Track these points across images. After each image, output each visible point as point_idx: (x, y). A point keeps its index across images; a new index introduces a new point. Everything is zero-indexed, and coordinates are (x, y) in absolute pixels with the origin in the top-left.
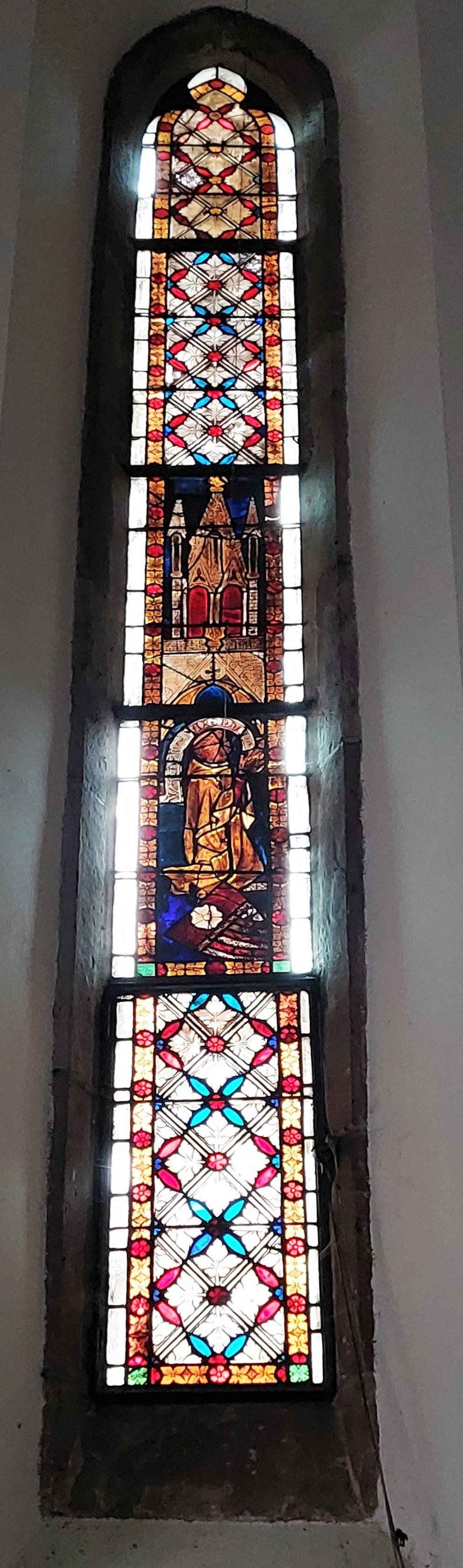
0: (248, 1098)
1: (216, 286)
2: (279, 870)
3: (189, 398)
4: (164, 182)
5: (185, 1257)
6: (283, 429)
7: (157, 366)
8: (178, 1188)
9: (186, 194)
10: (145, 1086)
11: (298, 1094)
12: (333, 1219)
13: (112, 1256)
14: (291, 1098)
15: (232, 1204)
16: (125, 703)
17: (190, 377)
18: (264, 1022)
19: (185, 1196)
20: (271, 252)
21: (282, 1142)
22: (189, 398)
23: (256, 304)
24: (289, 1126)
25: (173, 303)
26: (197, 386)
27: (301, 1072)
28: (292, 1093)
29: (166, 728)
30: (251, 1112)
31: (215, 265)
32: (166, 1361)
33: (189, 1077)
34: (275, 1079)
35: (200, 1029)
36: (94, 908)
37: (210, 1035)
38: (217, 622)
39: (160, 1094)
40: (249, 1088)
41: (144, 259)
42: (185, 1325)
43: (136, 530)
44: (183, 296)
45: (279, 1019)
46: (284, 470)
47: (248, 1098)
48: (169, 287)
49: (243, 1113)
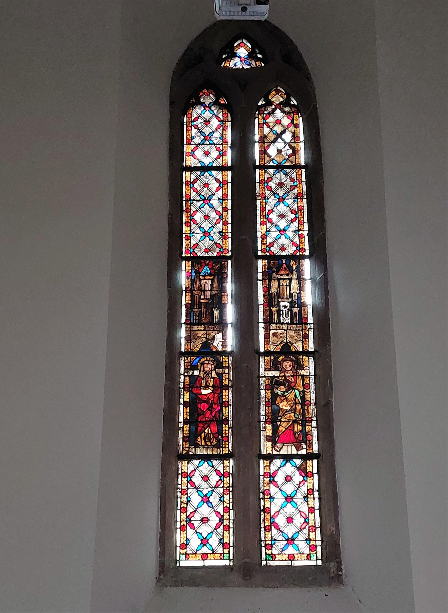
0: (214, 233)
1: (207, 153)
4: (305, 306)
6: (216, 560)
9: (196, 145)
15: (201, 507)
17: (200, 209)
18: (219, 179)
19: (196, 531)
26: (201, 198)
27: (180, 532)
28: (301, 197)
29: (186, 450)
31: (207, 161)
32: (200, 521)
33: (198, 467)
40: (215, 230)
43: (181, 422)
45: (222, 178)
47: (214, 233)
49: (202, 466)
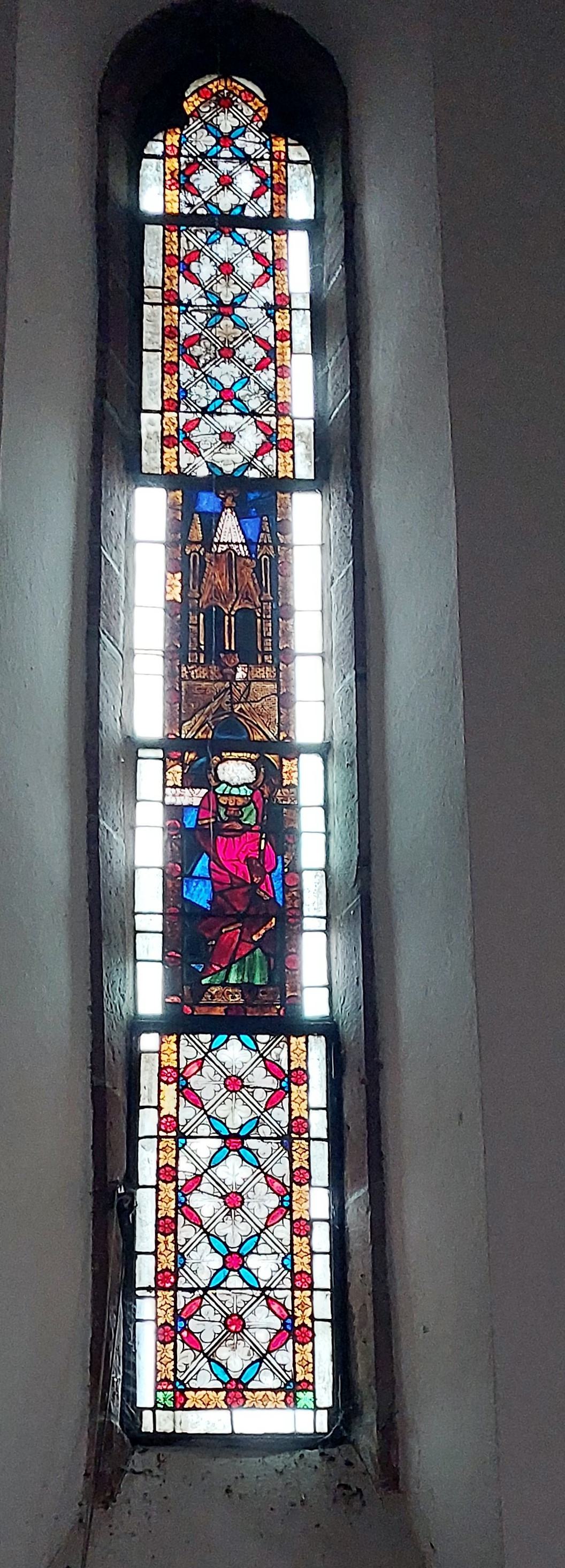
1: (226, 182)
2: (286, 741)
3: (204, 1148)
5: (206, 1167)
7: (170, 436)
8: (200, 817)
10: (165, 1228)
11: (306, 1136)
12: (323, 274)
13: (140, 550)
14: (300, 1138)
16: (143, 1430)
20: (279, 232)
21: (292, 1181)
22: (204, 1148)
23: (266, 293)
24: (298, 1217)
25: (187, 291)
30: (264, 1149)
33: (208, 1235)
34: (285, 1123)
35: (218, 1067)
36: (112, 923)
37: (229, 1313)
38: (233, 648)
39: (183, 1131)
41: (153, 236)
42: (205, 1227)
44: (194, 279)
46: (291, 484)
48: (181, 270)
